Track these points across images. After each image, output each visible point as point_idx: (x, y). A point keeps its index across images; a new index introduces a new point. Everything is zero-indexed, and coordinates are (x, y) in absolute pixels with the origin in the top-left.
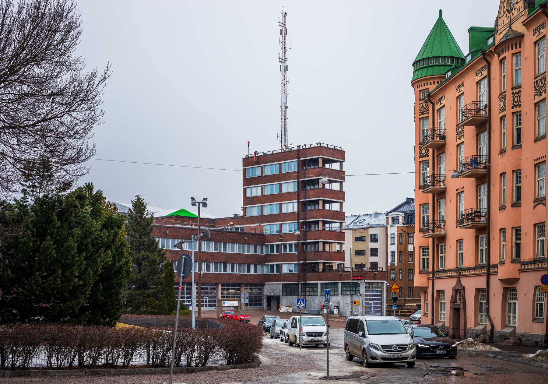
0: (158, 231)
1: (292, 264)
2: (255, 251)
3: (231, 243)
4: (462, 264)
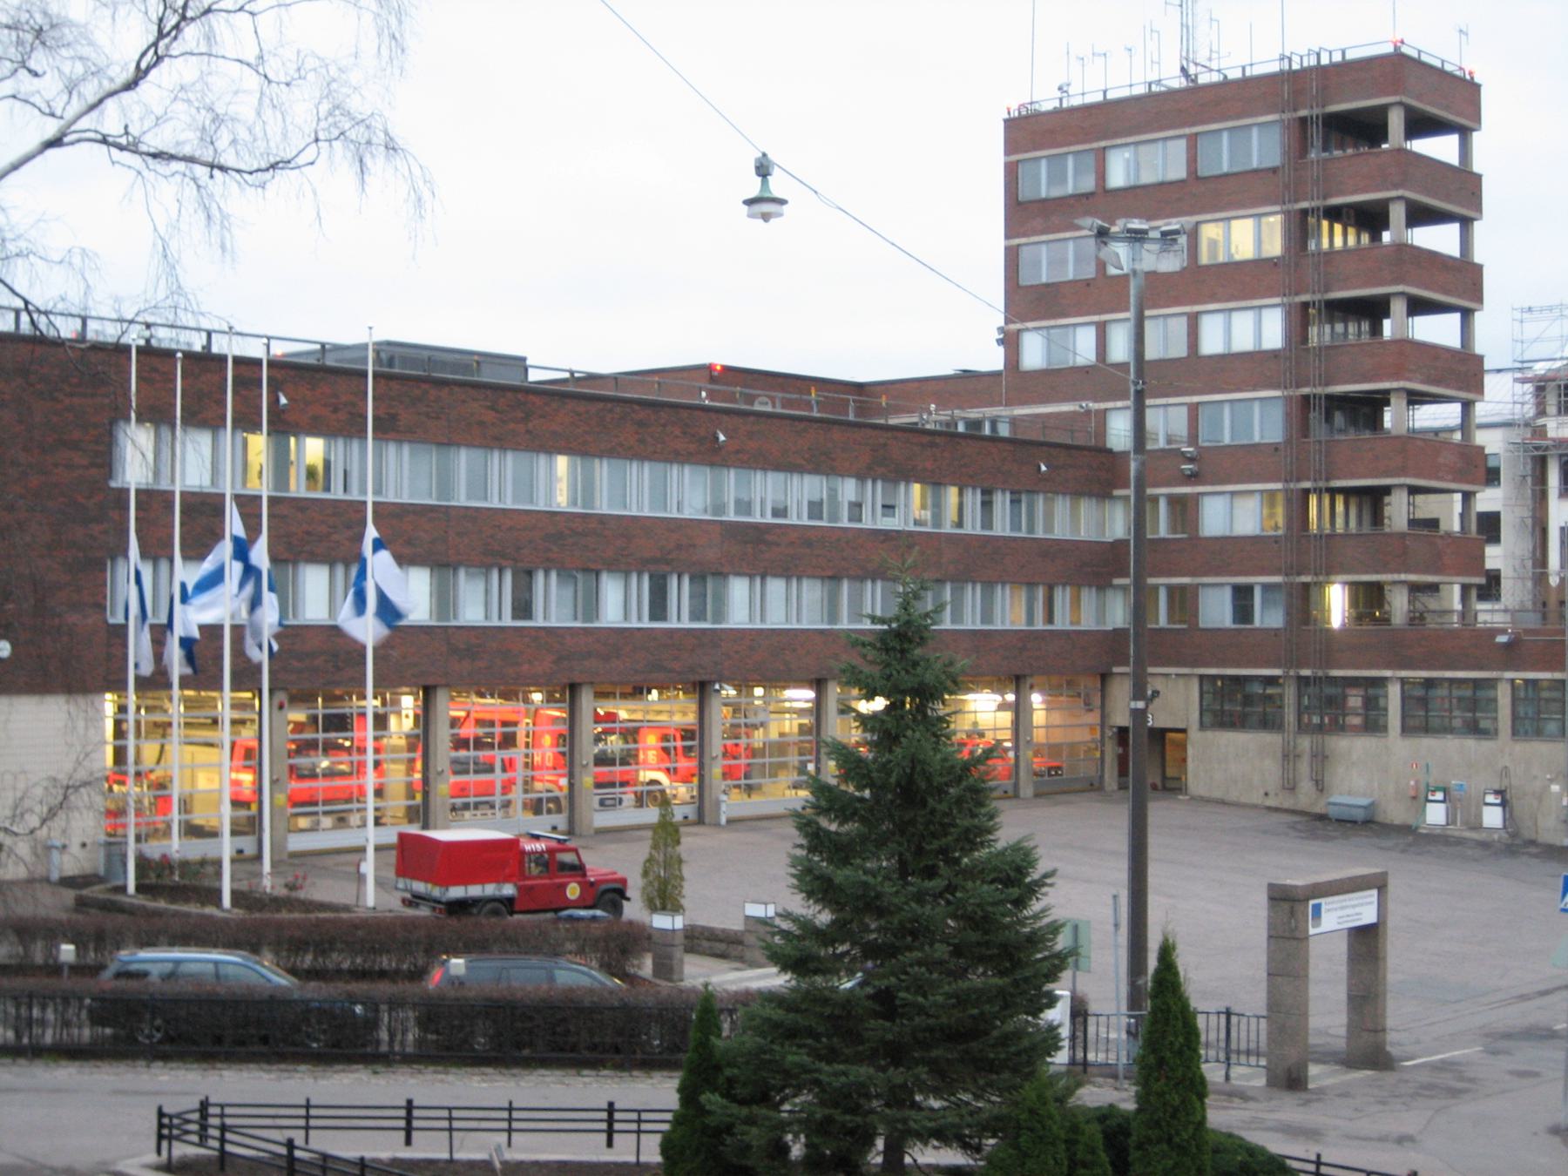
0: (677, 432)
1: (1222, 585)
2: (987, 522)
3: (884, 480)
4: (763, 620)
